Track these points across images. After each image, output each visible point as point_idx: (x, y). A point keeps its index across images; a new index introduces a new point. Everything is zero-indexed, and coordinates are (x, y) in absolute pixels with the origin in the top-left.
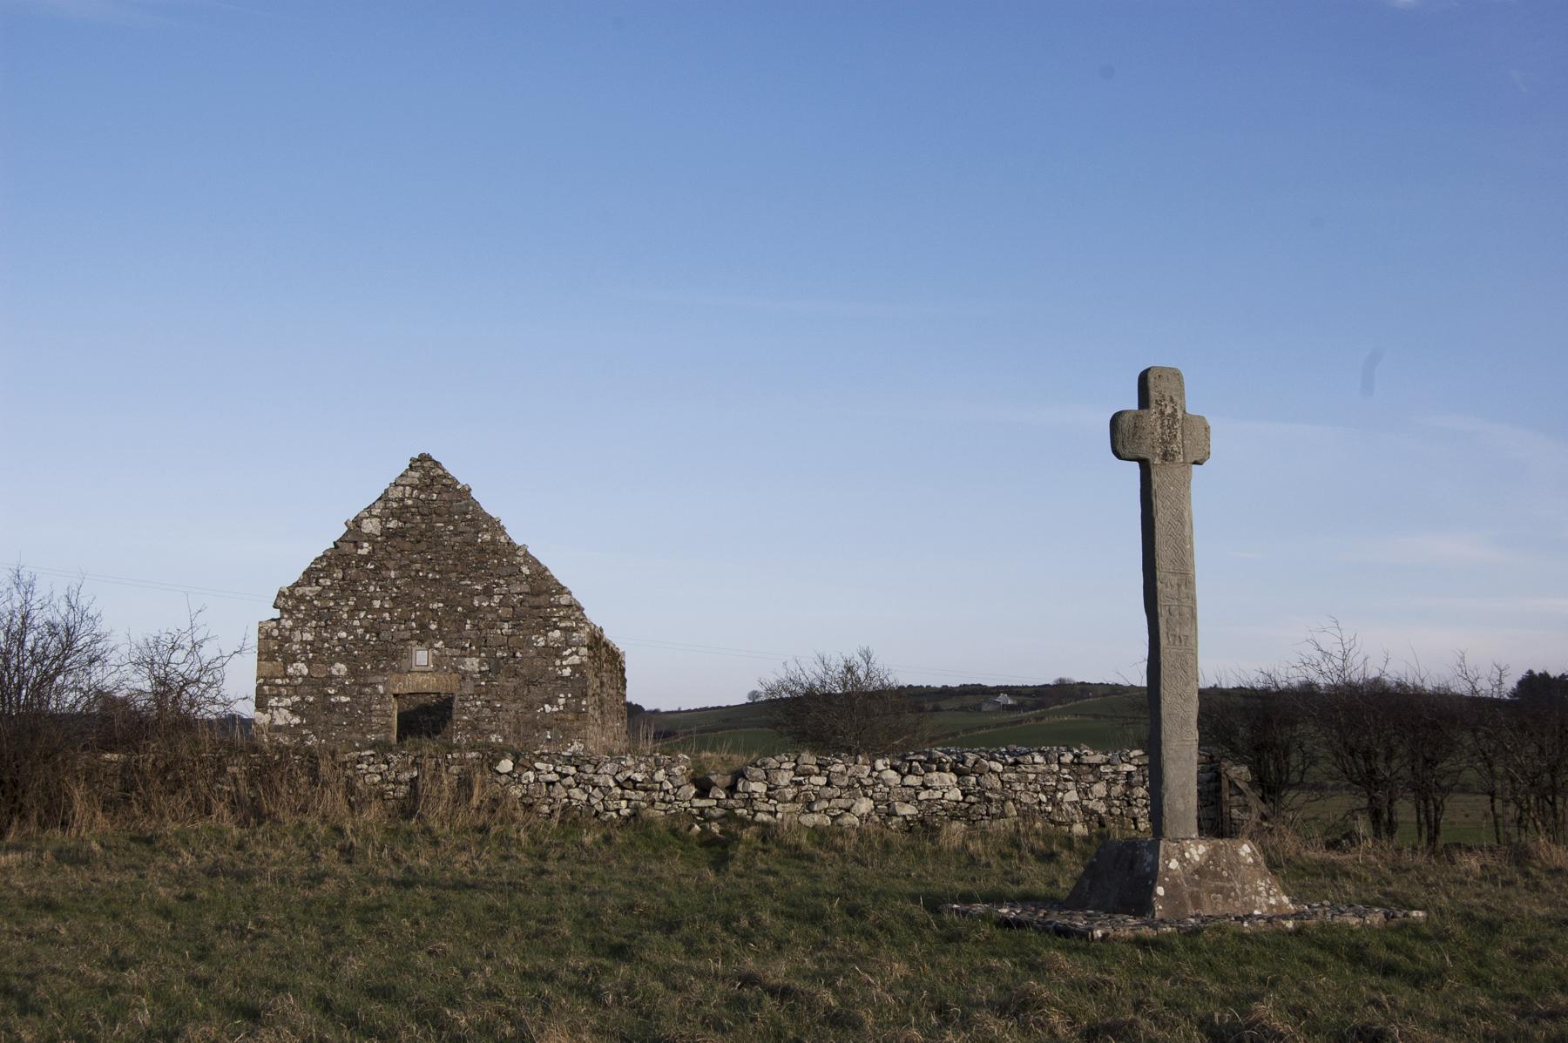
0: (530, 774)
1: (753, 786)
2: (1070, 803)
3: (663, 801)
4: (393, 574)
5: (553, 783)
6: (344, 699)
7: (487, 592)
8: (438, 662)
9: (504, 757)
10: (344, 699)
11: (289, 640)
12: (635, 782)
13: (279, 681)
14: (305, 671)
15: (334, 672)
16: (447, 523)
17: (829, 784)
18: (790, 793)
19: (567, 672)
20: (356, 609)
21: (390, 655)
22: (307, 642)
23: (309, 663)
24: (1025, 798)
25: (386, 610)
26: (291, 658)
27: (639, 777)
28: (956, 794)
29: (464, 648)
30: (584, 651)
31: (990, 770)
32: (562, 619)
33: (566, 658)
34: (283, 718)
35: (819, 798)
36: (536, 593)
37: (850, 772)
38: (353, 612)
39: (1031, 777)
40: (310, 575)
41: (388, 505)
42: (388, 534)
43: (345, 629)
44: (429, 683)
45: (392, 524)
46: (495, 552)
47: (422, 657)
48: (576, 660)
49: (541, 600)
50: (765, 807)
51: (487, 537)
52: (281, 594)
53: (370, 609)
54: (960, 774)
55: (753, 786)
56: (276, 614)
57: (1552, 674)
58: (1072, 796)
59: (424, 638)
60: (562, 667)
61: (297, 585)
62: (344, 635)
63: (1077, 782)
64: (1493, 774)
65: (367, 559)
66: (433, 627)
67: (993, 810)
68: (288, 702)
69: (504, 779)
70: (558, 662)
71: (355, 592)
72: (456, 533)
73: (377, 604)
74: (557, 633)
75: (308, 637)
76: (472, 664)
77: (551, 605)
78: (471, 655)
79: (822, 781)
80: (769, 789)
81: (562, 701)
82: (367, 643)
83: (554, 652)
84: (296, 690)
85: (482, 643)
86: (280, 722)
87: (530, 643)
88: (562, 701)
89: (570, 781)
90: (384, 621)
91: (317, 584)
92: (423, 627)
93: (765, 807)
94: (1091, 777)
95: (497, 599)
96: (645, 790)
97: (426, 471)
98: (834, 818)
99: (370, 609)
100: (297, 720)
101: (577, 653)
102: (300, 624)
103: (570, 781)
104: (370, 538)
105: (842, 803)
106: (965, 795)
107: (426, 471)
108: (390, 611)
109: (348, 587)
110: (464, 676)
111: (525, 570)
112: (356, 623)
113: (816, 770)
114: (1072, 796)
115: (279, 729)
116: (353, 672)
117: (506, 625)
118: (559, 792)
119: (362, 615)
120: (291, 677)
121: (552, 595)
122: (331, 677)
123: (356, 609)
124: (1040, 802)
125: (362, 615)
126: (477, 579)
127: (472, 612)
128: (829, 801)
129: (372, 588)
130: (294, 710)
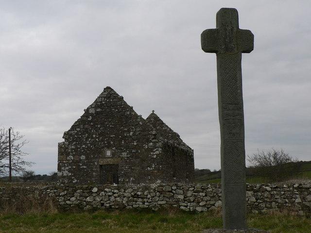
0: (103, 192)
1: (179, 197)
2: (298, 203)
3: (147, 202)
4: (99, 126)
5: (111, 196)
6: (85, 167)
7: (129, 131)
8: (113, 154)
9: (95, 186)
10: (85, 167)
11: (67, 148)
12: (138, 195)
13: (65, 162)
14: (73, 158)
15: (81, 158)
16: (115, 109)
17: (206, 196)
18: (192, 199)
19: (155, 156)
20: (88, 138)
21: (99, 152)
22: (73, 149)
23: (74, 155)
24: (280, 201)
25: (97, 138)
26: (68, 154)
27: (139, 193)
28: (254, 199)
29: (122, 150)
30: (160, 149)
31: (266, 190)
32: (153, 139)
33: (154, 152)
34: (66, 173)
35: (202, 200)
36: (144, 130)
37: (214, 191)
38: (87, 139)
39: (283, 193)
40: (73, 127)
41: (97, 104)
42: (97, 113)
43: (84, 144)
44: (110, 161)
45: (99, 110)
46: (131, 118)
47: (109, 153)
48: (157, 152)
49: (146, 133)
50: (184, 204)
51: (128, 113)
52: (65, 134)
53: (92, 138)
54: (255, 191)
55: (179, 197)
56: (63, 140)
57: (48, 175)
58: (298, 200)
59: (109, 147)
60: (153, 155)
61: (69, 131)
62: (84, 146)
63: (300, 194)
64: (79, 207)
65: (91, 121)
66: (112, 143)
67: (268, 205)
68: (67, 168)
69: (94, 195)
70: (152, 153)
71: (87, 132)
72: (119, 112)
73: (94, 136)
74: (151, 144)
75: (73, 147)
76: (124, 154)
77: (149, 134)
78: (124, 151)
79: (204, 194)
80: (185, 198)
81: (153, 166)
82: (91, 149)
83: (151, 150)
84: (70, 164)
85: (127, 148)
86: (65, 175)
87: (143, 147)
88: (153, 166)
89: (116, 195)
90: (96, 141)
91: (76, 130)
92: (109, 143)
93: (184, 204)
94: (306, 193)
95: (131, 133)
96: (142, 198)
97: (108, 90)
98: (208, 208)
99: (92, 138)
100: (70, 174)
101: (158, 150)
102: (70, 143)
103: (116, 195)
104: (92, 114)
105: (212, 203)
106: (257, 200)
107: (108, 90)
108: (98, 138)
109: (86, 131)
110: (122, 158)
111: (141, 123)
112: (88, 142)
113: (201, 190)
114: (298, 200)
115: (64, 177)
116: (87, 158)
117: (135, 142)
118: (112, 198)
119: (90, 139)
120: (68, 160)
121: (149, 131)
122: (80, 160)
123: (88, 138)
124: (286, 202)
125: (90, 139)
126: (125, 127)
127: (124, 138)
128: (206, 202)
129: (92, 131)
130: (69, 171)
